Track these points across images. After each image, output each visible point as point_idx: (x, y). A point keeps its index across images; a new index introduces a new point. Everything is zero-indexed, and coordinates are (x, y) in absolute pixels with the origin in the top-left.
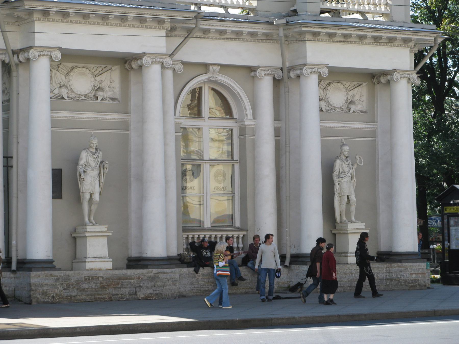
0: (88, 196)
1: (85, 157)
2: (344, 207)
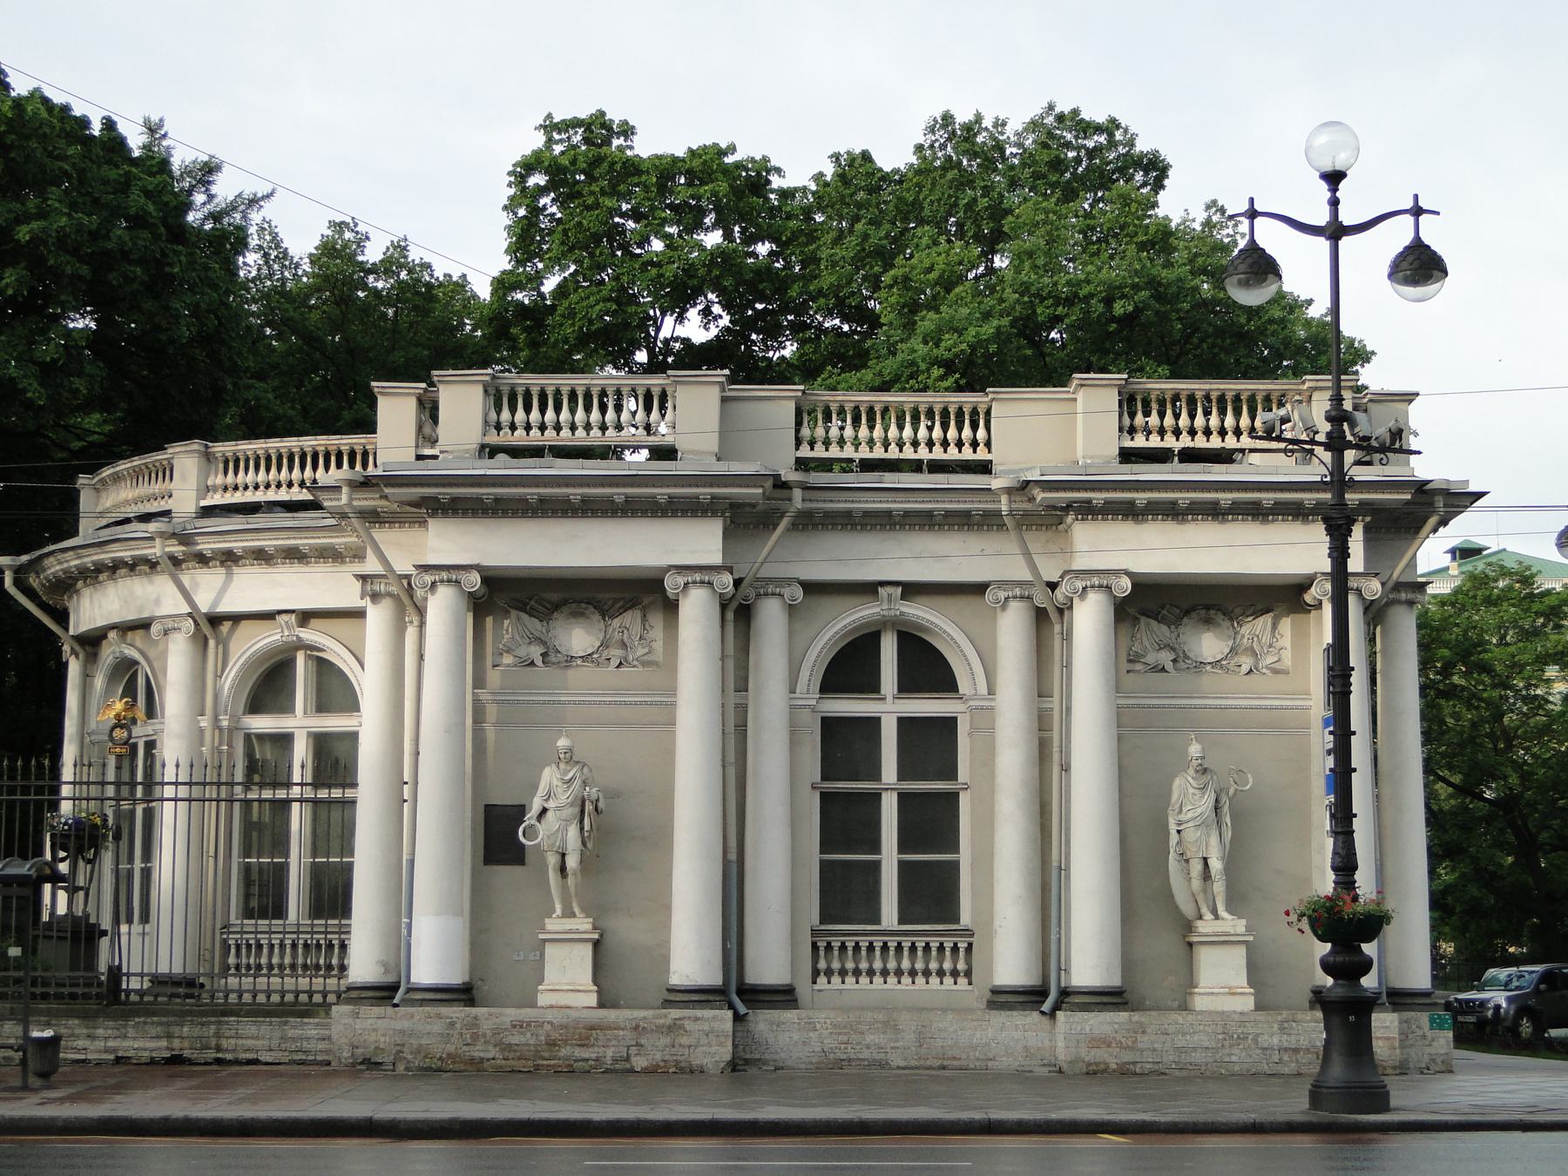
0: (552, 860)
1: (549, 776)
2: (1196, 883)
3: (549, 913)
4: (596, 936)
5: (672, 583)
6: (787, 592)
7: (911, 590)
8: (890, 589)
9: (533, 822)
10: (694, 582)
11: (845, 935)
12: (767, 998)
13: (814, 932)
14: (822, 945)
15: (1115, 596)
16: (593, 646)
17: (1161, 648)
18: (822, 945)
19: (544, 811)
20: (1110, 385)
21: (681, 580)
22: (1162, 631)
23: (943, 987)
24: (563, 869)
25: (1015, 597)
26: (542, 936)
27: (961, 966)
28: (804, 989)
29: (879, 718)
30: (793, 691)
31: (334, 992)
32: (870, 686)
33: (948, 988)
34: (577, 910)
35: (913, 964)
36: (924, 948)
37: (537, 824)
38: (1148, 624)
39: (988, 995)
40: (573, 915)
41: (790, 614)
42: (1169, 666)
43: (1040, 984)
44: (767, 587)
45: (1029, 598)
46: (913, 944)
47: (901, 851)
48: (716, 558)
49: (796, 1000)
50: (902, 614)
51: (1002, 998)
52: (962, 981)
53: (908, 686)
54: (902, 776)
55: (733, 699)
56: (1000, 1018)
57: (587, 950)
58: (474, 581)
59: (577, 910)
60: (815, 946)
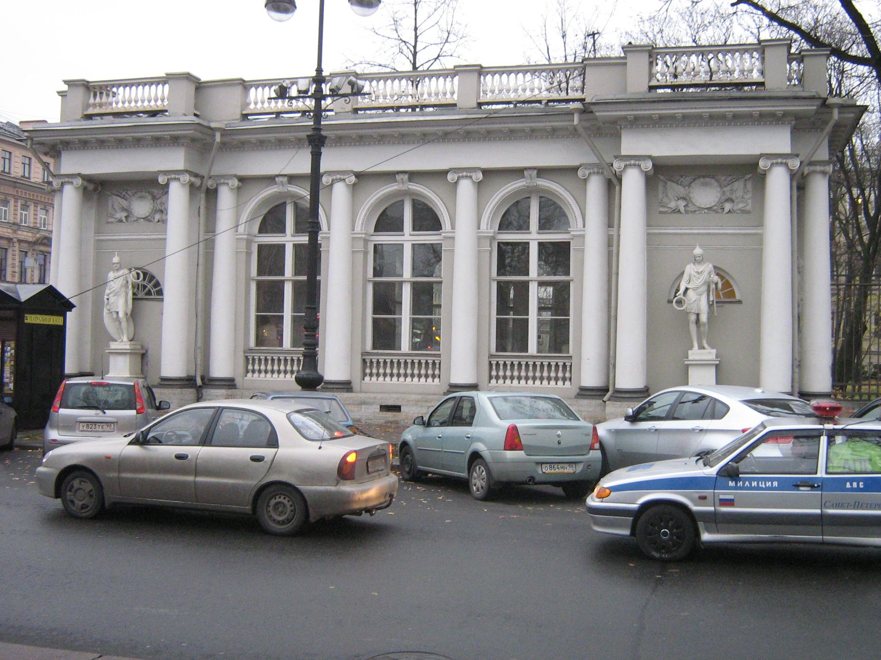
0: (693, 318)
3: (691, 348)
4: (718, 362)
5: (162, 180)
6: (230, 182)
7: (413, 175)
8: (530, 172)
9: (681, 296)
10: (630, 165)
11: (273, 353)
12: (218, 383)
13: (491, 356)
14: (494, 363)
15: (791, 170)
16: (715, 201)
17: (678, 199)
18: (494, 363)
19: (687, 289)
20: (779, 45)
21: (769, 163)
22: (681, 190)
23: (519, 385)
24: (698, 321)
25: (594, 173)
26: (686, 363)
27: (567, 375)
28: (356, 385)
29: (403, 244)
30: (479, 228)
31: (866, 394)
32: (524, 226)
33: (515, 385)
34: (706, 345)
35: (406, 371)
36: (511, 365)
37: (684, 298)
38: (116, 199)
39: (578, 391)
40: (704, 348)
41: (238, 194)
42: (682, 209)
43: (605, 385)
44: (222, 178)
45: (602, 173)
46: (549, 363)
47: (497, 315)
48: (787, 150)
49: (352, 388)
50: (289, 191)
51: (585, 393)
52: (437, 380)
53: (417, 226)
54: (260, 273)
55: (613, 232)
56: (585, 402)
57: (713, 371)
58: (648, 165)
59: (706, 345)
60: (491, 364)
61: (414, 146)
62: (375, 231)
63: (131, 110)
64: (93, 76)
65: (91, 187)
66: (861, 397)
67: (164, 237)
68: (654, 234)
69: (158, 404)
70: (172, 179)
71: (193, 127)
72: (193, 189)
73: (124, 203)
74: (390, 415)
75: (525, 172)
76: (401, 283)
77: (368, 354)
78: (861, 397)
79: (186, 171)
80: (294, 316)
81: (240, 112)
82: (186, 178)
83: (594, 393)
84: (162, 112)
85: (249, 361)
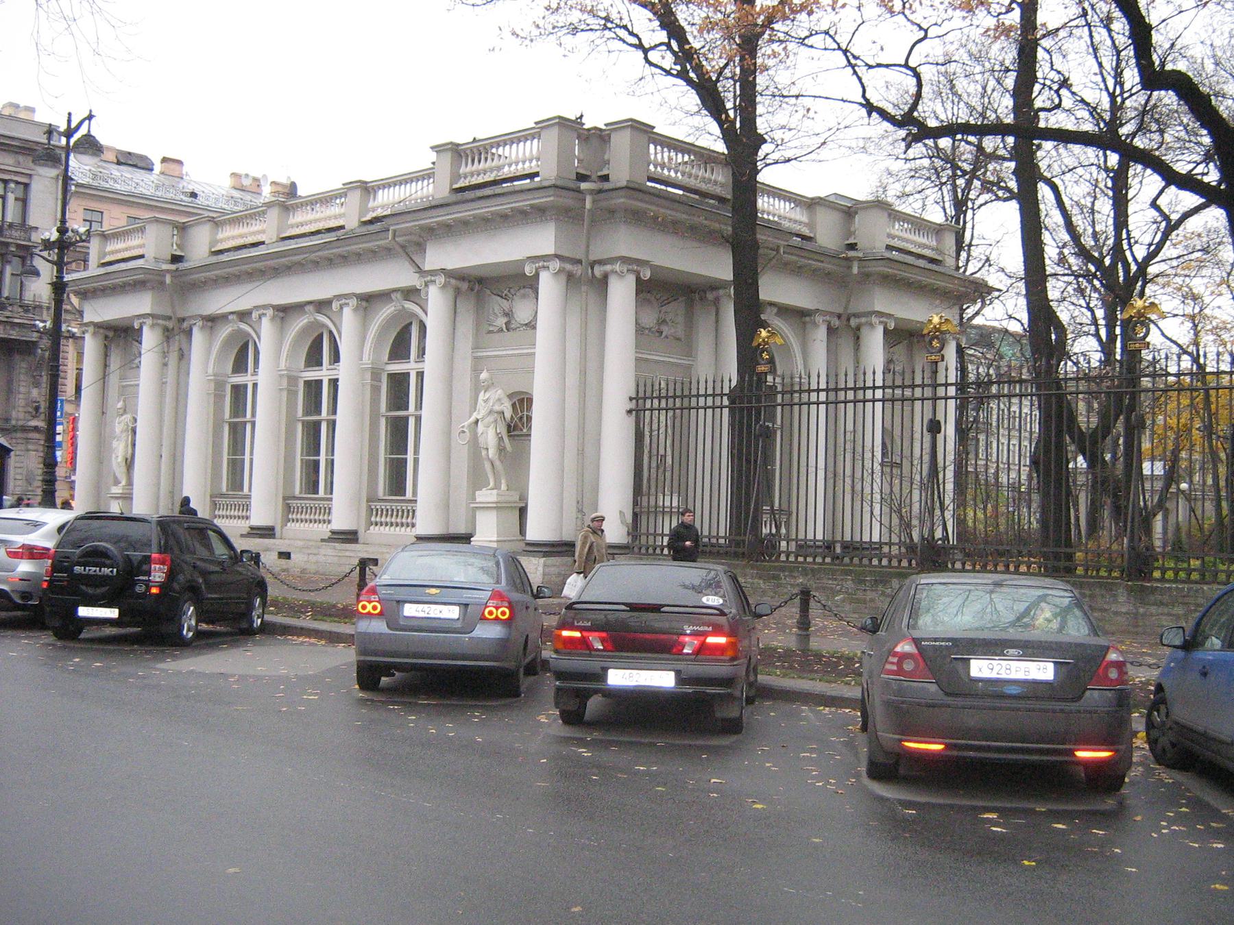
54: (389, 409)
61: (258, 284)
62: (389, 359)
63: (518, 174)
64: (463, 138)
65: (111, 334)
66: (1163, 573)
67: (532, 351)
68: (481, 358)
69: (535, 591)
70: (540, 267)
71: (551, 192)
72: (571, 280)
73: (505, 304)
74: (283, 562)
75: (393, 296)
76: (245, 423)
77: (222, 495)
78: (1163, 573)
79: (557, 256)
80: (308, 461)
81: (357, 219)
82: (556, 265)
83: (559, 549)
84: (537, 174)
85: (289, 507)
